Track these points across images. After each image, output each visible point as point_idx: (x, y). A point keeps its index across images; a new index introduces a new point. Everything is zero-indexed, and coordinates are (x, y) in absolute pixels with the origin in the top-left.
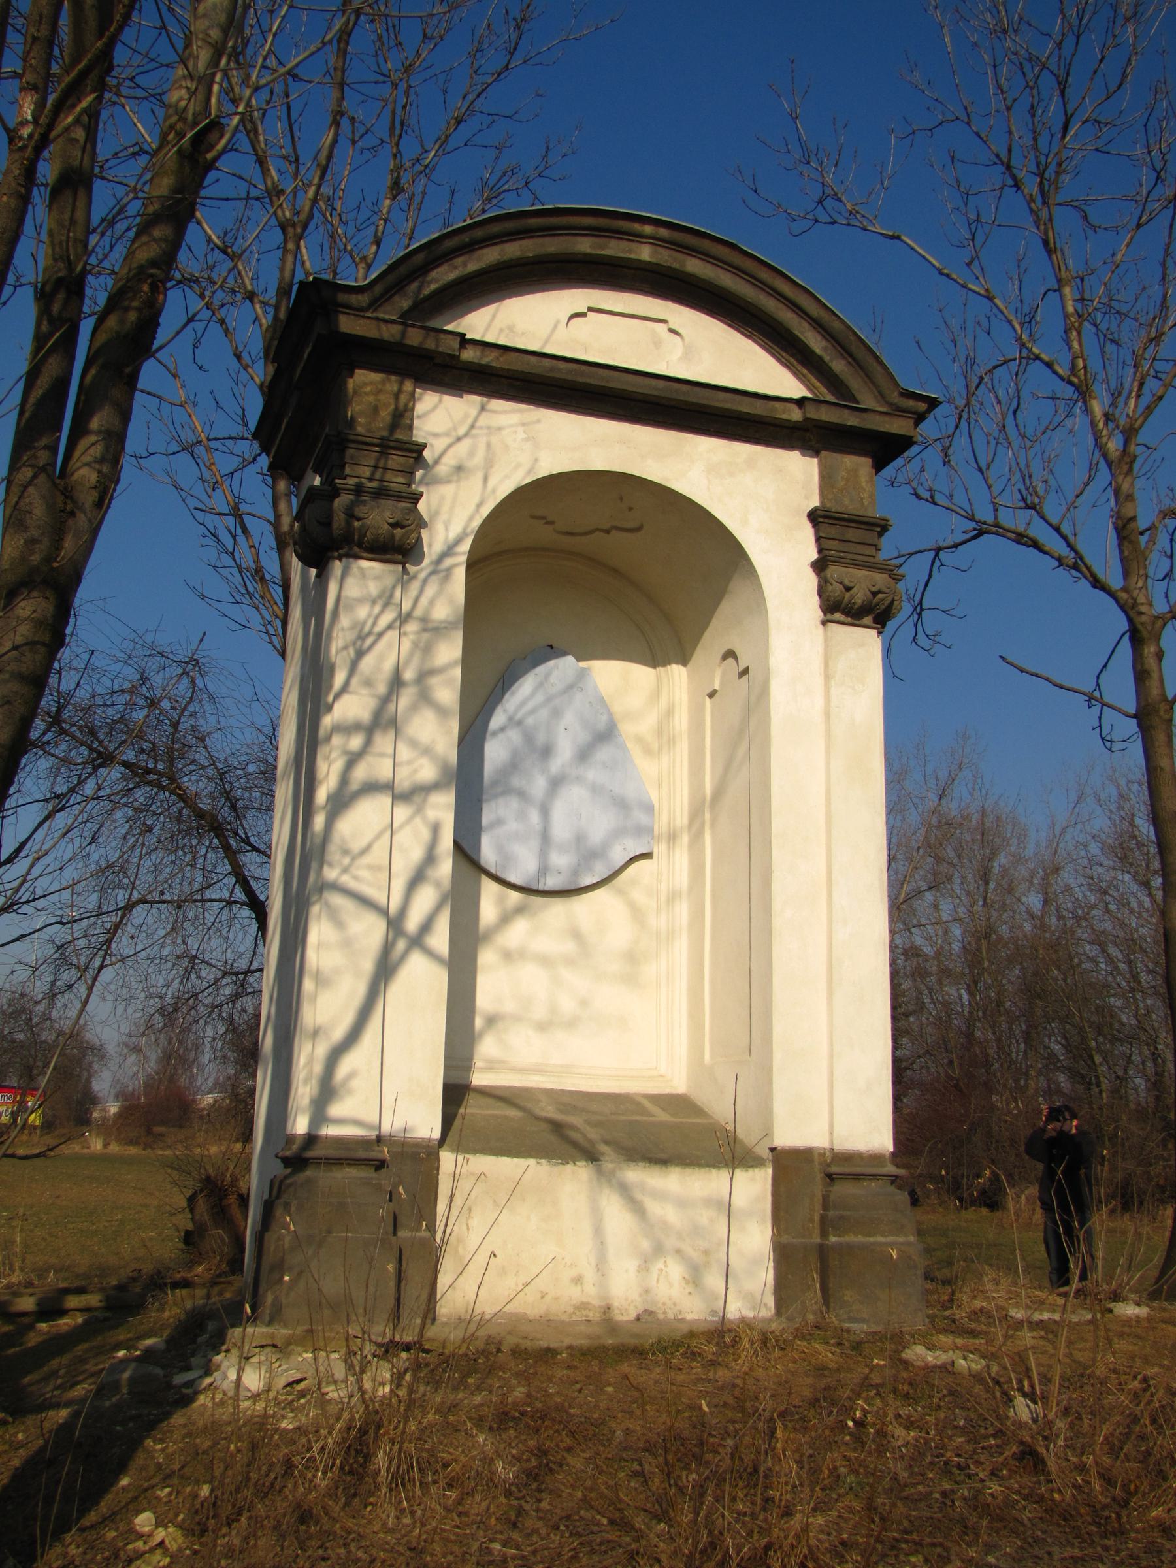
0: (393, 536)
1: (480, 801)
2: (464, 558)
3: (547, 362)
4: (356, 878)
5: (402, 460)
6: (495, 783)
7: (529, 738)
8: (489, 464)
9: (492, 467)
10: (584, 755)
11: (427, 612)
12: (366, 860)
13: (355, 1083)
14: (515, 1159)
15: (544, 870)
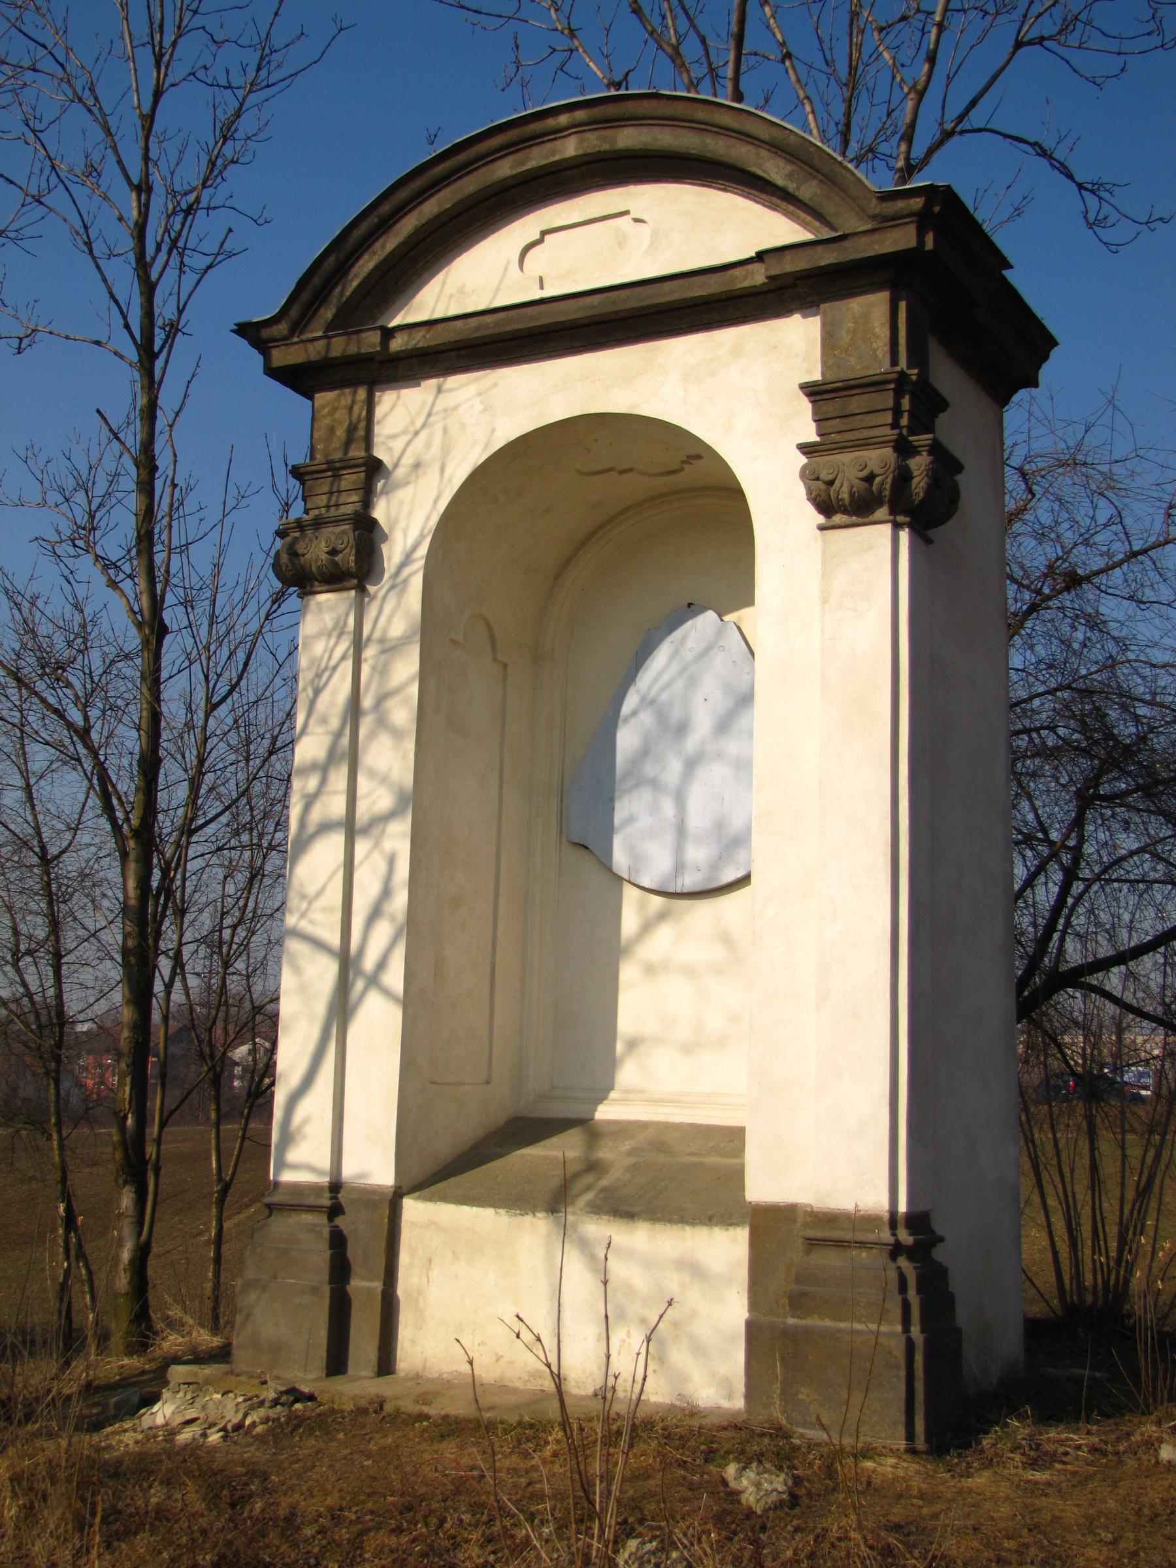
0: (335, 564)
1: (612, 800)
2: (422, 563)
3: (474, 322)
4: (312, 922)
5: (354, 477)
6: (628, 774)
7: (662, 717)
8: (446, 451)
9: (448, 454)
10: (723, 726)
11: (385, 631)
12: (321, 903)
13: (309, 1129)
14: (475, 1209)
15: (679, 867)
